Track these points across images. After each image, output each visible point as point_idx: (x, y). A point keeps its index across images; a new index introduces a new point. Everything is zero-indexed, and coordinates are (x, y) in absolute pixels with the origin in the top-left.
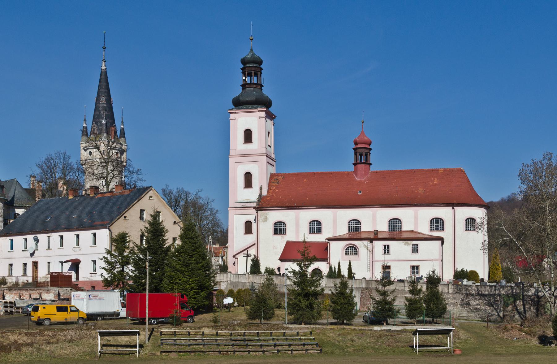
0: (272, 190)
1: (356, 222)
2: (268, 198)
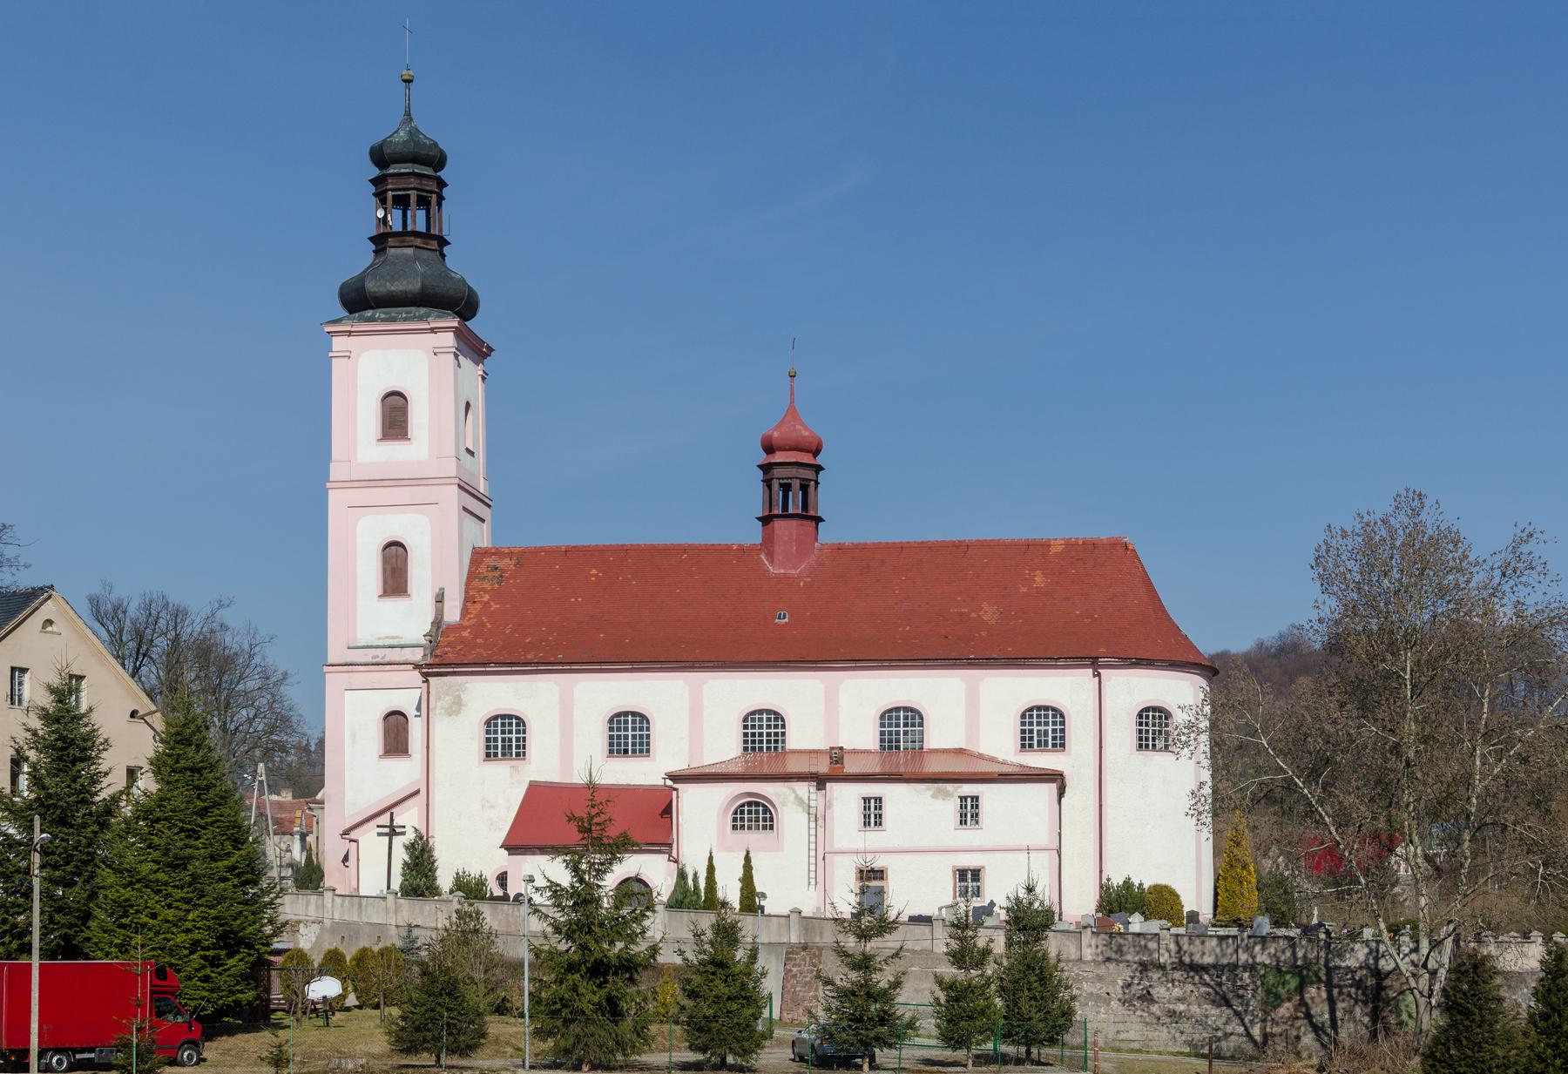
1: (769, 720)
2: (465, 634)
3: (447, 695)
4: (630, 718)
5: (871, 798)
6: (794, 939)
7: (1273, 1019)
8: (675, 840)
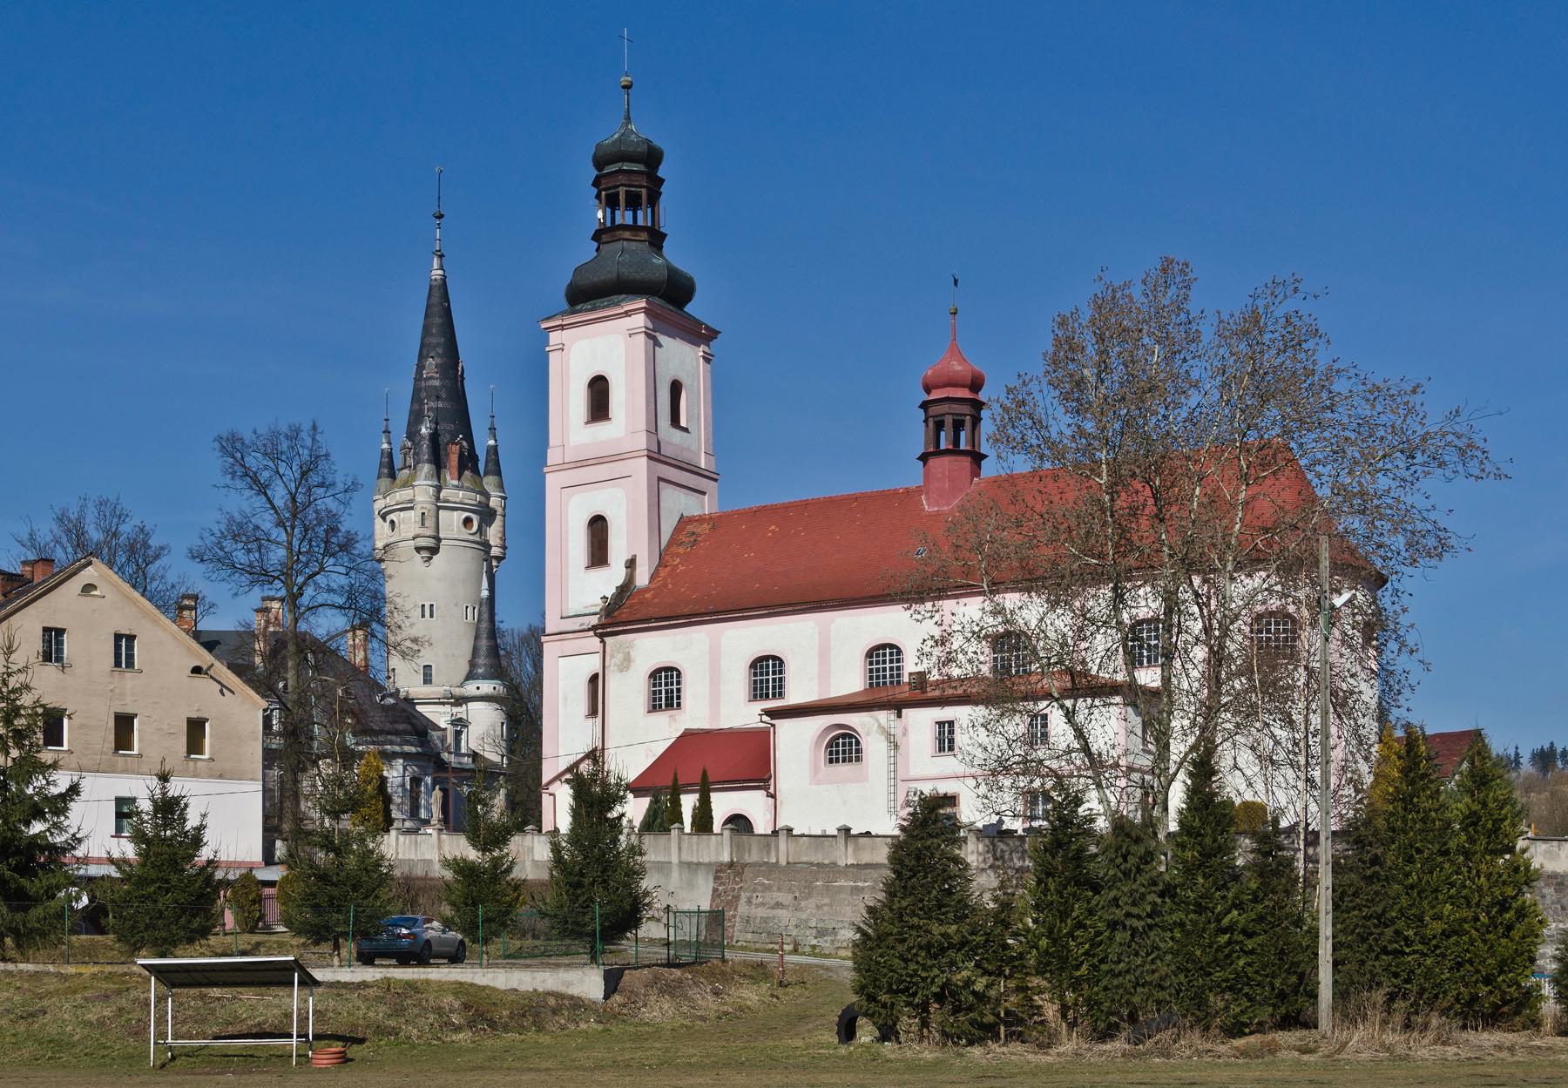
0: (669, 568)
1: (891, 654)
2: (648, 595)
5: (945, 722)
6: (726, 858)
7: (183, 858)
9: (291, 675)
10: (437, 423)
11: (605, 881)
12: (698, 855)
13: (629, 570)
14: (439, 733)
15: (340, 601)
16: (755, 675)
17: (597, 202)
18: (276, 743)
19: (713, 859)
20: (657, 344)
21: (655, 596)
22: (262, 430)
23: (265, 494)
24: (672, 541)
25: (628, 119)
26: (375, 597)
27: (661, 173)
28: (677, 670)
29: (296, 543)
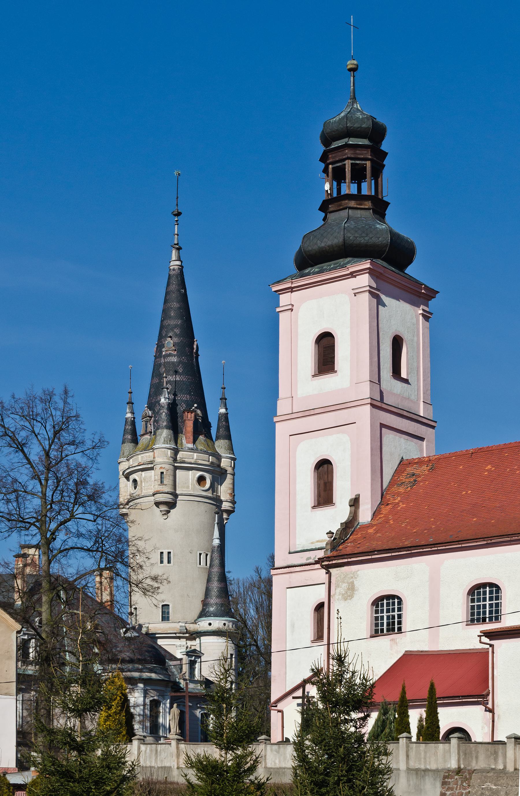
3: (343, 582)
4: (488, 589)
6: (453, 764)
8: (491, 692)
9: (44, 609)
10: (175, 395)
11: (349, 781)
12: (425, 762)
13: (353, 508)
14: (175, 663)
15: (89, 544)
16: (473, 601)
17: (324, 175)
18: (31, 670)
19: (440, 767)
20: (380, 303)
21: (377, 532)
22: (20, 395)
23: (23, 451)
24: (392, 483)
25: (354, 99)
26: (119, 541)
27: (384, 147)
28: (399, 598)
29: (49, 493)
